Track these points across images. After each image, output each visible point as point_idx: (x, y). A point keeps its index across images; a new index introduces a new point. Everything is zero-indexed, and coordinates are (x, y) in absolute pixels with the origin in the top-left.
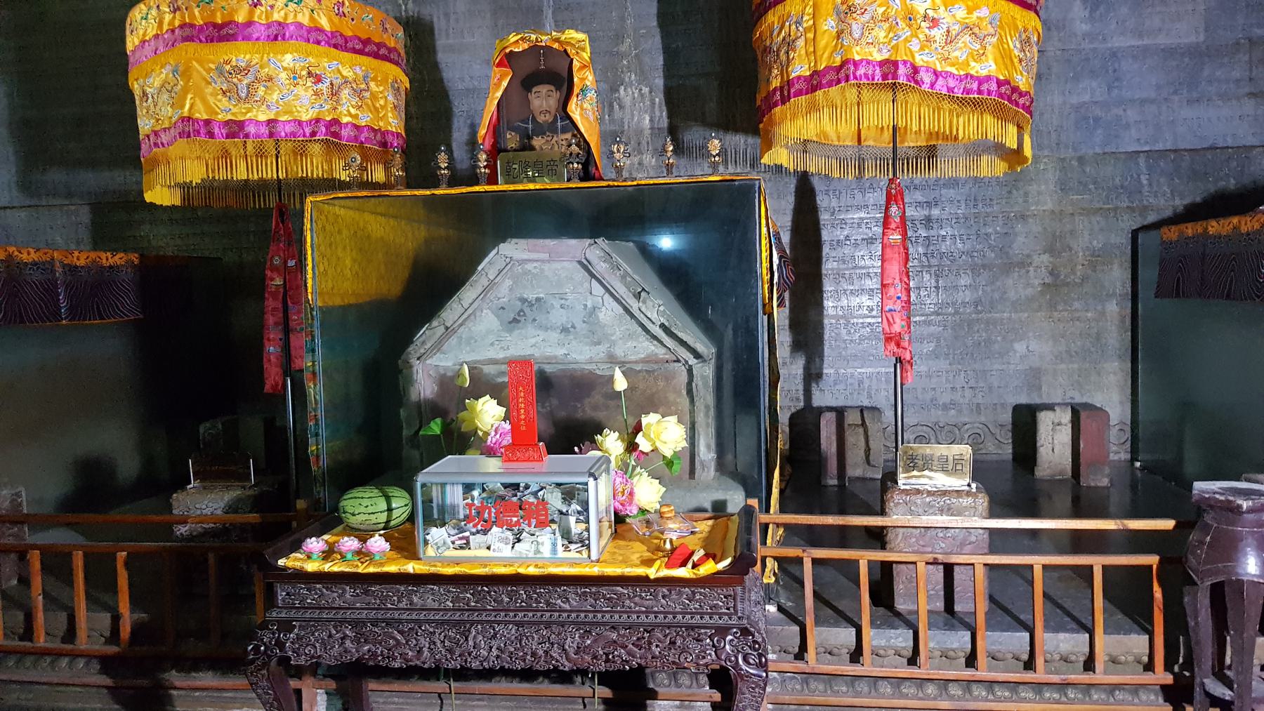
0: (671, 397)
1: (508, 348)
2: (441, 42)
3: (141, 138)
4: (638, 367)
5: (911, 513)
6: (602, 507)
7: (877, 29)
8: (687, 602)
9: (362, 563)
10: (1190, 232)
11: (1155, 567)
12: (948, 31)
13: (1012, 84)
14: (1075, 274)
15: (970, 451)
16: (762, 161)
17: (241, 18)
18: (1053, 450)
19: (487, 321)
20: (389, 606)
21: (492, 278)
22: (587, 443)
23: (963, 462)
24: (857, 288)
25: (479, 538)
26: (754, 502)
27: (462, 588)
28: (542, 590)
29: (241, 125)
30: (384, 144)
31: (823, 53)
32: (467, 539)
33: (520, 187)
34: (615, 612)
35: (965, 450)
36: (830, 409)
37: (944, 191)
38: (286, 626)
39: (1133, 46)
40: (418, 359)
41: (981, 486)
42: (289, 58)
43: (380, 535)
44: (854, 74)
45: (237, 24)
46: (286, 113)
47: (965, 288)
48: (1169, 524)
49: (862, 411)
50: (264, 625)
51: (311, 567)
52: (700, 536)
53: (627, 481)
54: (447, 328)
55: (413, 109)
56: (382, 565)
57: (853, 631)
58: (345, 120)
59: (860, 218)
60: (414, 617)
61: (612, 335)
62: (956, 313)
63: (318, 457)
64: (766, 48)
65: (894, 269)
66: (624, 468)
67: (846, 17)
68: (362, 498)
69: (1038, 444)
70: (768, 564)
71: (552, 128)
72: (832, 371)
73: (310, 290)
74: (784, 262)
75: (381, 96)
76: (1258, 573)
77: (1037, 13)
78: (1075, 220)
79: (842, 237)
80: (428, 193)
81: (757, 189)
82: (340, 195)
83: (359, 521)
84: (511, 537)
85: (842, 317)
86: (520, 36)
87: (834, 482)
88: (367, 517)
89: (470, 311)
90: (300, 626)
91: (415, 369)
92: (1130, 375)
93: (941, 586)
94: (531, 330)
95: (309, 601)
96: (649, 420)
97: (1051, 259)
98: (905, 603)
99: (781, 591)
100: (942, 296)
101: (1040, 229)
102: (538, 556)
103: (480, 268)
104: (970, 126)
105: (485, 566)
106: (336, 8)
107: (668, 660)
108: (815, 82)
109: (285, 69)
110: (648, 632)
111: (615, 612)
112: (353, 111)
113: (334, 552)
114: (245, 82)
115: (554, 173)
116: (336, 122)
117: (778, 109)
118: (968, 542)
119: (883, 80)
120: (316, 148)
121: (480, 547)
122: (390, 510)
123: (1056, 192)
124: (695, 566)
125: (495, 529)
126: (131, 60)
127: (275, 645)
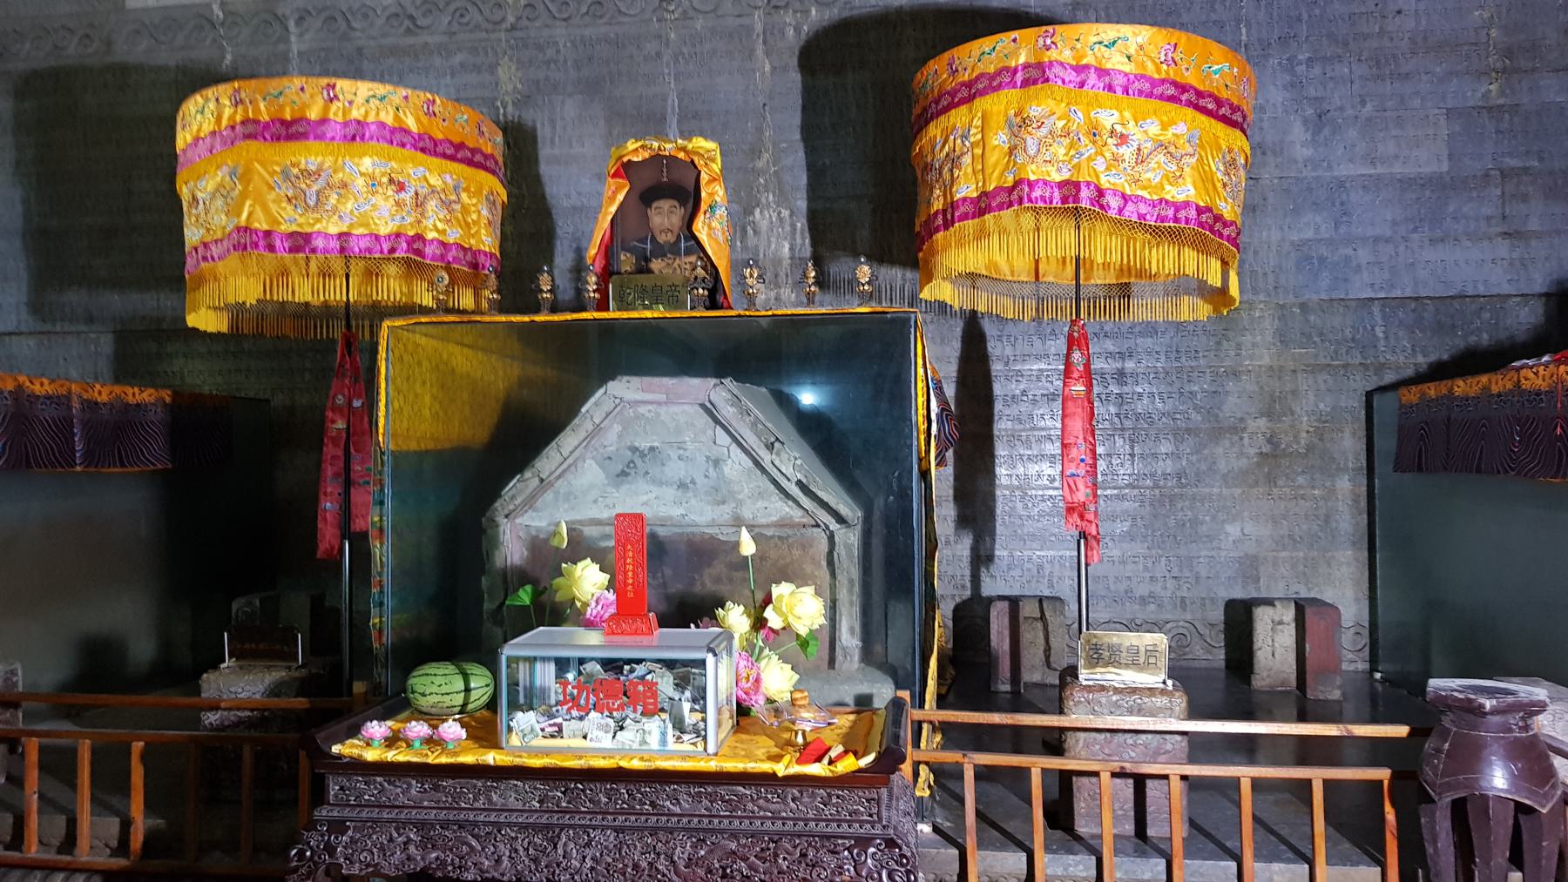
0: (809, 568)
1: (614, 506)
2: (544, 152)
3: (187, 250)
4: (769, 532)
5: (1094, 712)
6: (723, 697)
7: (1055, 145)
8: (822, 806)
9: (433, 752)
10: (1432, 393)
11: (1386, 783)
12: (1139, 150)
13: (1215, 212)
14: (1298, 443)
15: (1165, 641)
16: (921, 296)
17: (313, 114)
18: (1273, 655)
19: (591, 473)
20: (463, 805)
21: (597, 422)
22: (706, 619)
23: (1157, 654)
24: (1035, 453)
25: (575, 724)
26: (905, 694)
27: (551, 784)
28: (648, 789)
29: (307, 237)
30: (475, 266)
31: (993, 172)
32: (560, 727)
33: (635, 315)
34: (735, 817)
35: (1160, 640)
36: (1002, 598)
37: (1139, 341)
38: (338, 827)
39: (1364, 175)
40: (507, 516)
41: (1177, 683)
42: (368, 162)
43: (454, 720)
44: (1029, 196)
45: (308, 121)
46: (361, 225)
47: (1166, 457)
48: (1402, 731)
49: (1041, 601)
50: (311, 825)
51: (371, 755)
52: (840, 731)
53: (752, 664)
54: (542, 480)
55: (509, 229)
56: (456, 754)
57: (1023, 856)
58: (430, 235)
59: (1040, 370)
60: (492, 819)
61: (739, 493)
62: (1156, 486)
63: (380, 631)
64: (926, 164)
65: (1077, 426)
66: (750, 648)
67: (1019, 131)
68: (435, 675)
69: (1256, 647)
70: (921, 772)
71: (674, 249)
72: (1005, 553)
73: (381, 430)
74: (947, 415)
75: (473, 209)
76: (1505, 787)
77: (1244, 131)
78: (1297, 378)
79: (1018, 392)
80: (526, 319)
81: (912, 324)
82: (423, 320)
83: (431, 703)
84: (612, 724)
85: (1018, 488)
86: (640, 144)
87: (1007, 688)
88: (439, 698)
89: (570, 461)
90: (355, 828)
91: (501, 529)
92: (1367, 567)
93: (1130, 805)
94: (642, 485)
95: (367, 797)
96: (781, 590)
97: (1269, 425)
98: (1086, 826)
99: (938, 810)
100: (1139, 466)
101: (1257, 389)
102: (644, 747)
103: (584, 410)
104: (1164, 259)
105: (580, 758)
106: (425, 106)
107: (797, 876)
108: (982, 205)
109: (362, 174)
110: (773, 842)
111: (735, 817)
112: (440, 226)
113: (399, 739)
114: (315, 188)
115: (677, 304)
116: (419, 237)
117: (940, 236)
118: (1163, 751)
119: (1063, 203)
120: (392, 269)
121: (574, 736)
122: (467, 690)
123: (1274, 344)
124: (831, 762)
125: (593, 714)
126: (181, 159)
127: (324, 849)
